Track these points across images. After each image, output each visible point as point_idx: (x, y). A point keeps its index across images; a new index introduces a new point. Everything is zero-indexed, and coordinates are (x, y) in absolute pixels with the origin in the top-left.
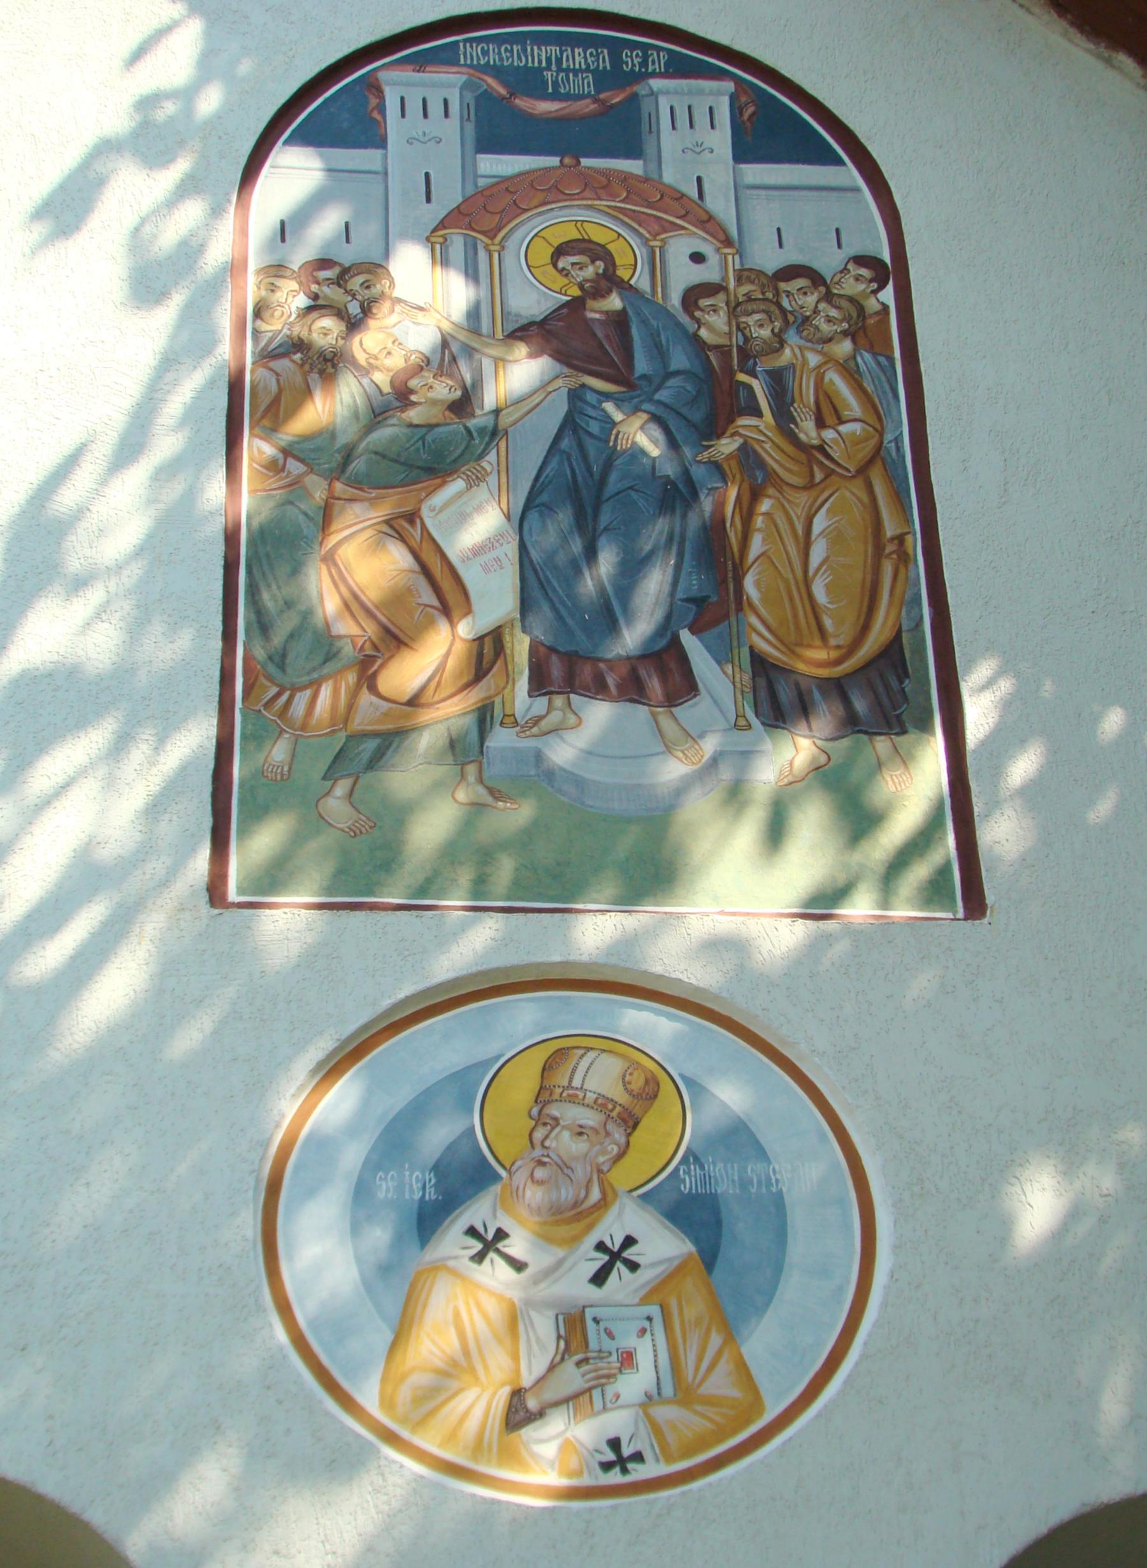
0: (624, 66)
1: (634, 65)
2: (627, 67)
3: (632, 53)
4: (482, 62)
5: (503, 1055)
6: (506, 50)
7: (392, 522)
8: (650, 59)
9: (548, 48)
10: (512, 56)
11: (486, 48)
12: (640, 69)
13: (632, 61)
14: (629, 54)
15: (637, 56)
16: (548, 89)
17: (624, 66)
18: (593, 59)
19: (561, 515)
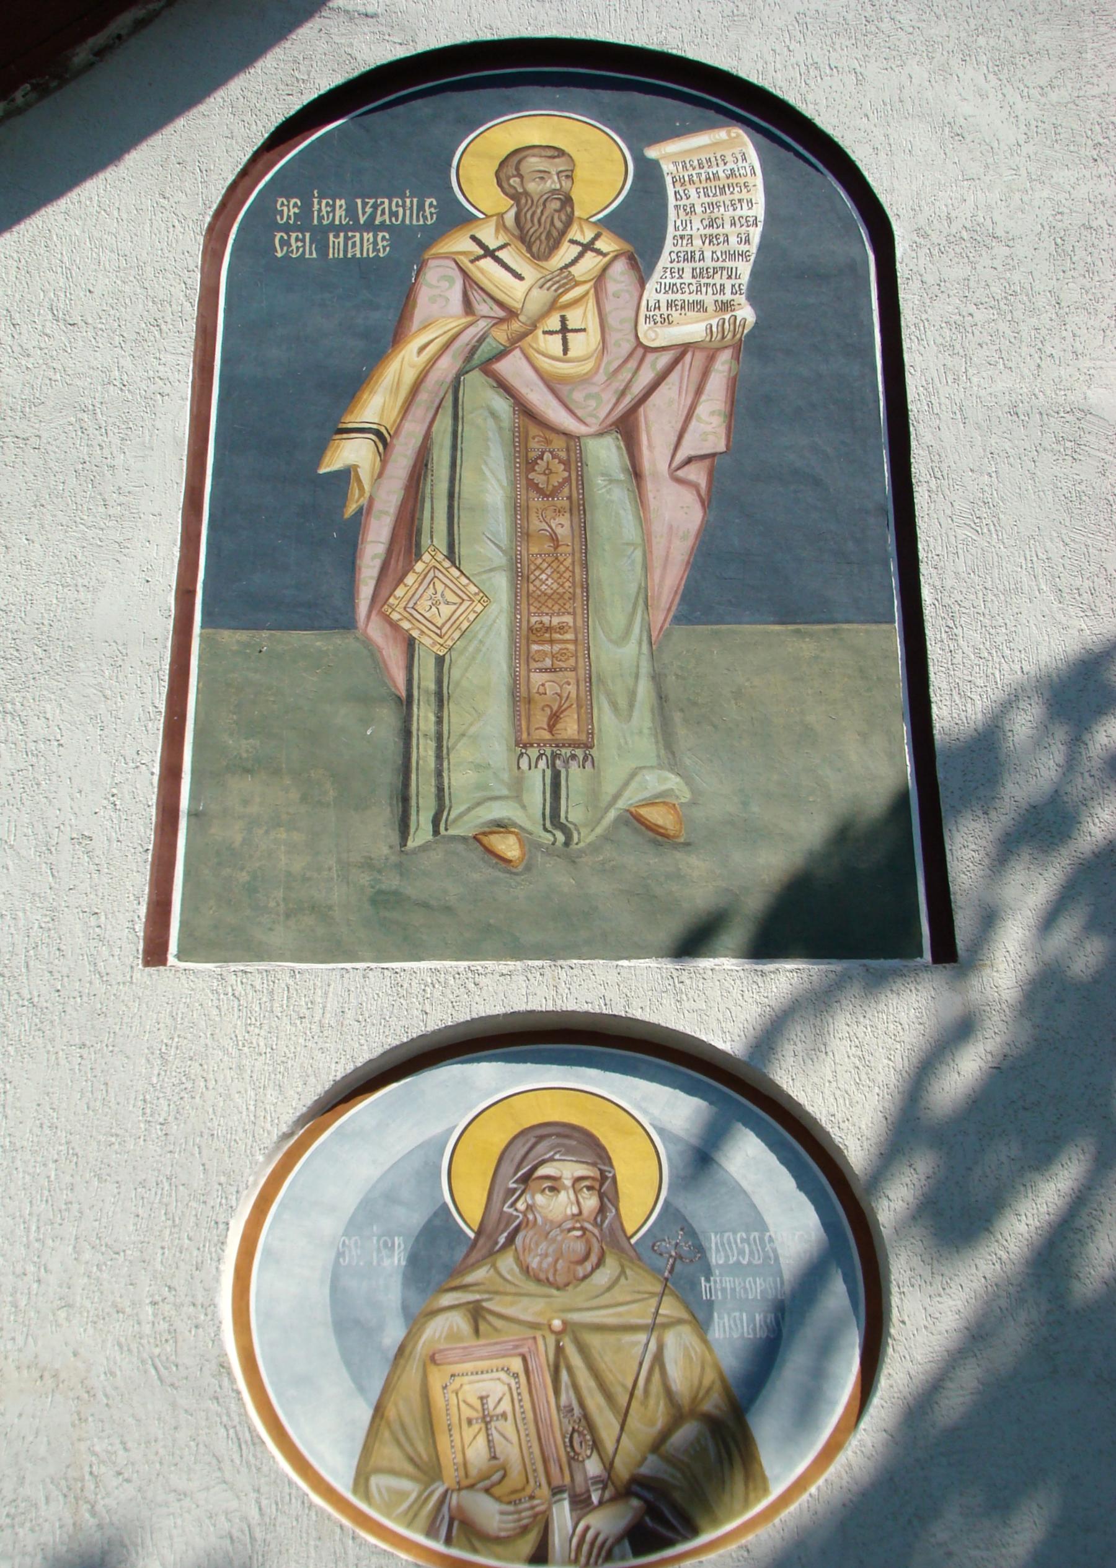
0: (278, 217)
1: (289, 217)
2: (282, 219)
3: (289, 202)
4: (371, 255)
5: (454, 1127)
6: (327, 204)
7: (485, 840)
8: (380, 209)
9: (421, 222)
10: (304, 246)
11: (393, 219)
12: (295, 221)
13: (289, 210)
14: (286, 203)
15: (295, 205)
16: (328, 255)
17: (278, 217)
18: (329, 209)
19: (386, 850)
